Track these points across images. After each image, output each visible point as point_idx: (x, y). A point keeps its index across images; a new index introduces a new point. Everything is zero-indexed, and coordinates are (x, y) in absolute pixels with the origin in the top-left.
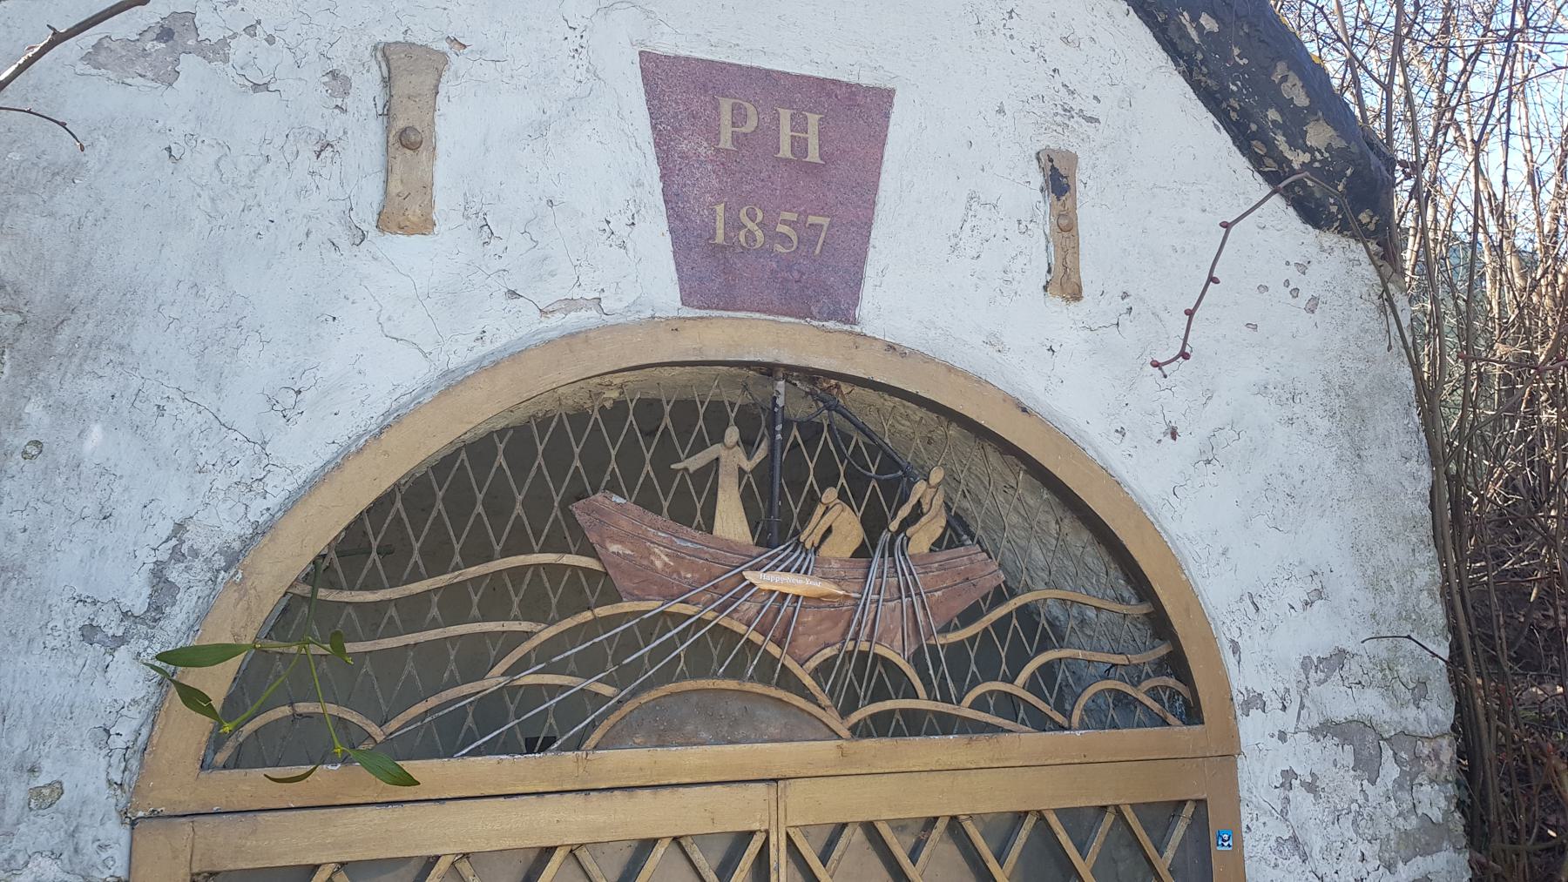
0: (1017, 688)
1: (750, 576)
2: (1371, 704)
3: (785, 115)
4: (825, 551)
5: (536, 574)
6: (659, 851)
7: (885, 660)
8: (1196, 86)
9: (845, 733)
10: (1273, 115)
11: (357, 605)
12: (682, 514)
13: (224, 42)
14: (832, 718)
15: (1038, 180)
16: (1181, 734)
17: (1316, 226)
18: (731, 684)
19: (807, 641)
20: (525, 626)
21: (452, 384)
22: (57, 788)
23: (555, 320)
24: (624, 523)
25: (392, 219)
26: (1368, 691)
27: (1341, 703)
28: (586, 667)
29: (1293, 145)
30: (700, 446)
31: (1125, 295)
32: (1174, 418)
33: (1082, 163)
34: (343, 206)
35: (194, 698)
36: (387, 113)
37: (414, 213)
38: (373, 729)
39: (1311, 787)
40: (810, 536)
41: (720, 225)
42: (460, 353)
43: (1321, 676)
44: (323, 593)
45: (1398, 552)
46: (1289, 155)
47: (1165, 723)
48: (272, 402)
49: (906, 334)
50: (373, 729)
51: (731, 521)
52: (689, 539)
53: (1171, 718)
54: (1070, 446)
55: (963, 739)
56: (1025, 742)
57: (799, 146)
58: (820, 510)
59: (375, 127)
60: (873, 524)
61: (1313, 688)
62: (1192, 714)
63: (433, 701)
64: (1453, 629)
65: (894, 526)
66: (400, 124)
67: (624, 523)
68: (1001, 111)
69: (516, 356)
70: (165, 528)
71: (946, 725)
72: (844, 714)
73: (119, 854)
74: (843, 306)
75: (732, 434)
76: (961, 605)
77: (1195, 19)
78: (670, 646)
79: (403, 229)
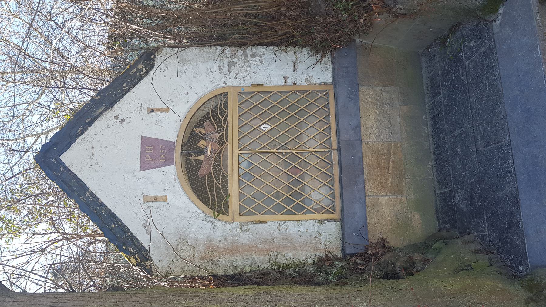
0: (223, 119)
1: (208, 155)
2: (226, 62)
3: (147, 151)
4: (205, 145)
5: (209, 182)
6: (240, 166)
7: (219, 137)
8: (134, 86)
9: (227, 143)
10: (138, 74)
11: (212, 202)
12: (201, 164)
13: (145, 220)
14: (226, 145)
15: (152, 114)
16: (229, 95)
17: (154, 66)
18: (221, 158)
19: (217, 148)
20: (214, 183)
21: (185, 192)
22: (230, 230)
23: (177, 181)
24: (202, 171)
25: (166, 201)
26: (224, 63)
27: (226, 68)
28: (218, 175)
29: (142, 71)
30: (192, 162)
31: (168, 100)
32: (186, 93)
33: (148, 106)
34: (164, 206)
35: (218, 216)
36: (152, 202)
37: (164, 198)
38: (225, 199)
39: (237, 74)
40: (203, 147)
41: (163, 160)
42: (182, 192)
43: (222, 70)
44: (210, 205)
45: (204, 54)
46: (144, 72)
47: (227, 98)
48: (189, 212)
49: (176, 134)
50: (225, 199)
51: (201, 158)
52: (204, 163)
53: (227, 97)
54: (190, 110)
55: (229, 127)
56: (229, 118)
57: (150, 149)
58: (200, 146)
59: (154, 203)
60: (201, 138)
61: (224, 72)
62: (226, 93)
63: (222, 193)
65: (202, 136)
66: (154, 200)
67: (202, 171)
68: (142, 119)
69: (182, 185)
70: (203, 222)
71: (227, 129)
72: (225, 143)
73: (237, 223)
75: (190, 158)
76: (212, 127)
77: (124, 87)
78: (216, 165)
79: (167, 199)
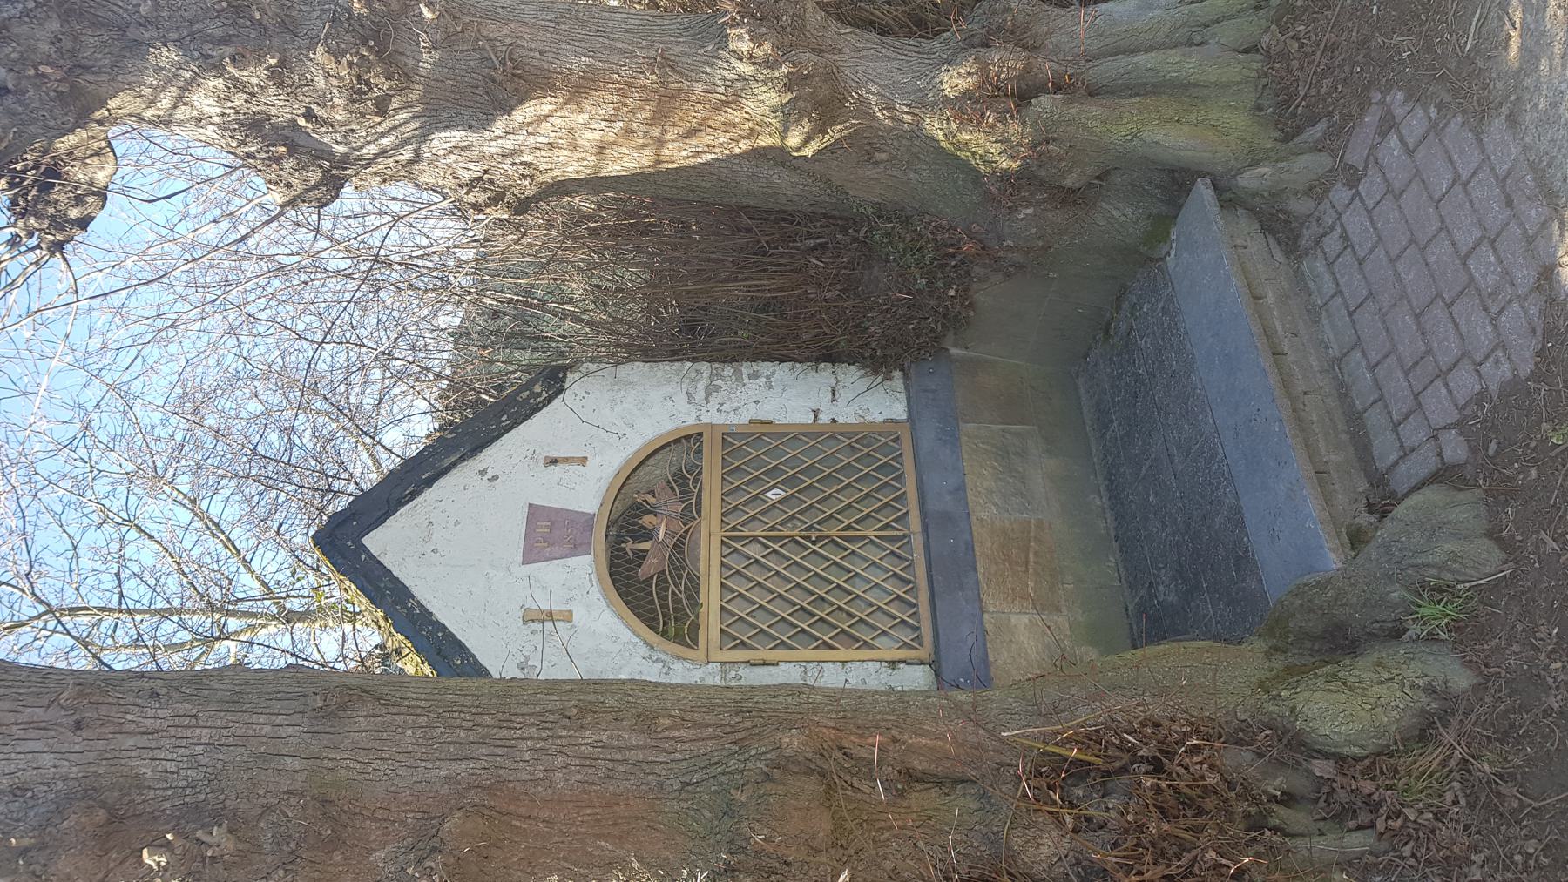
14: (696, 522)
21: (610, 604)
25: (568, 617)
28: (680, 577)
51: (646, 546)
64: (682, 360)
74: (588, 521)
